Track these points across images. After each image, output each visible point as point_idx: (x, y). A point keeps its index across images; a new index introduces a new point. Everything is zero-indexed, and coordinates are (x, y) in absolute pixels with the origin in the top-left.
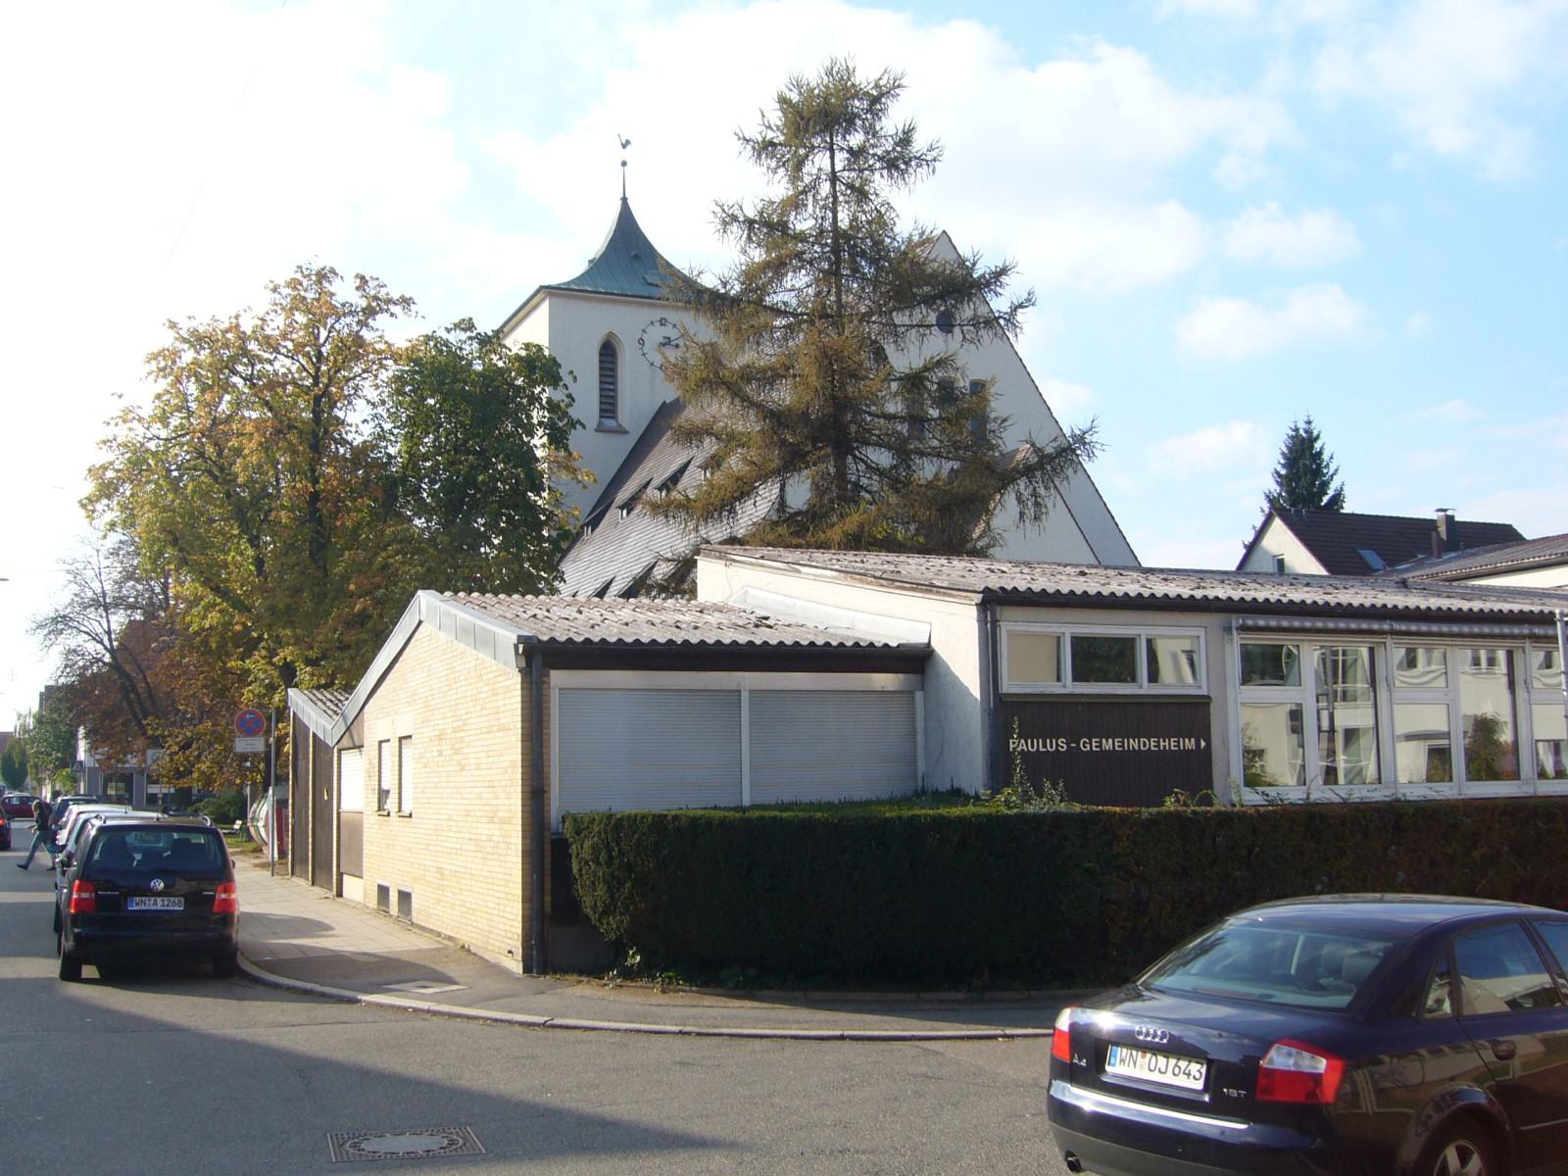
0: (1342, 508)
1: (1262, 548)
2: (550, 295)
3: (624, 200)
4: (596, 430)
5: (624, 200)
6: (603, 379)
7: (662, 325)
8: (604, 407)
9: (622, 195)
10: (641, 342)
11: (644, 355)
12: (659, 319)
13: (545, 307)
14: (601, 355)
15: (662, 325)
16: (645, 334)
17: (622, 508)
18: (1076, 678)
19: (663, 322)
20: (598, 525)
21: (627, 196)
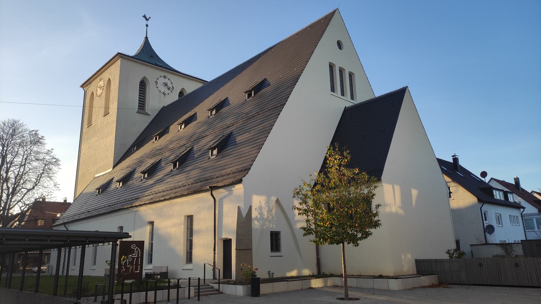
0: (348, 243)
1: (298, 274)
2: (121, 57)
3: (146, 38)
4: (137, 112)
5: (146, 38)
6: (140, 99)
7: (164, 78)
8: (140, 87)
9: (145, 36)
10: (156, 82)
11: (157, 87)
12: (163, 76)
13: (118, 63)
14: (140, 85)
15: (164, 78)
16: (158, 80)
17: (181, 124)
18: (138, 271)
19: (165, 77)
20: (353, 73)
21: (146, 27)
